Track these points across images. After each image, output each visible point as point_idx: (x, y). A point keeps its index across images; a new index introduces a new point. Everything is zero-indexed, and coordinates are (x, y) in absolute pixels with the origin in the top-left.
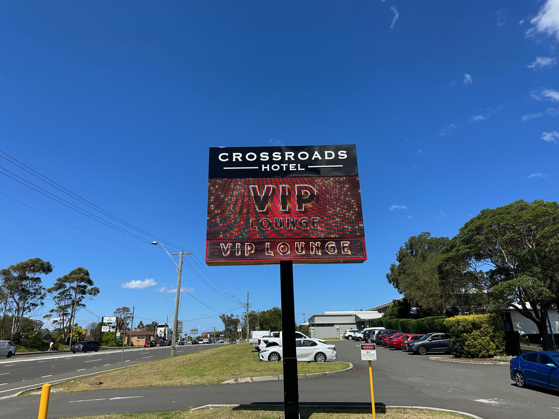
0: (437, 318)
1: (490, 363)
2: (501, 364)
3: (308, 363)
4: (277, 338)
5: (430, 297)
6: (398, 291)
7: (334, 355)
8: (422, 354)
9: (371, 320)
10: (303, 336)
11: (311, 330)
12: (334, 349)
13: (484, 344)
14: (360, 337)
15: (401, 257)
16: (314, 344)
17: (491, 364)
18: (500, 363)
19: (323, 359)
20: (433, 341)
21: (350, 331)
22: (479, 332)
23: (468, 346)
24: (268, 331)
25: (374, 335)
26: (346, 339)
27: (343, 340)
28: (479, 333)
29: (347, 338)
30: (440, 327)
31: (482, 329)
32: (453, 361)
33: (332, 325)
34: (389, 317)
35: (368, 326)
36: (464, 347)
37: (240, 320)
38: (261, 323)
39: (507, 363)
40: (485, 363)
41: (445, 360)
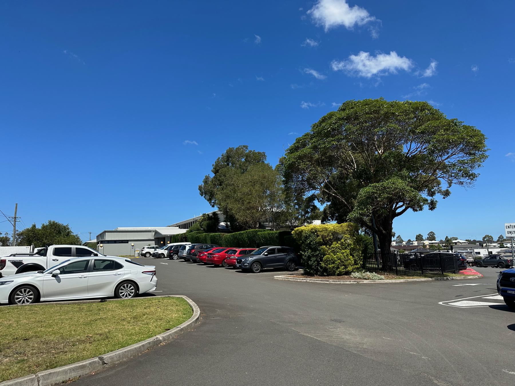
0: (259, 231)
1: (353, 282)
2: (364, 282)
3: (101, 302)
4: (42, 257)
5: (248, 209)
6: (211, 205)
7: (153, 283)
8: (255, 271)
9: (172, 236)
10: (93, 253)
11: (100, 248)
12: (154, 273)
13: (343, 259)
14: (163, 254)
15: (218, 168)
16: (116, 266)
17: (354, 283)
18: (363, 281)
19: (132, 293)
20: (269, 256)
21: (148, 248)
22: (339, 244)
23: (326, 261)
24: (30, 247)
25: (184, 250)
26: (142, 257)
27: (138, 257)
28: (340, 246)
29: (144, 255)
30: (263, 240)
31: (343, 240)
32: (308, 281)
33: (126, 242)
34: (197, 232)
35: (169, 242)
36: (321, 262)
37: (10, 239)
38: (29, 239)
39: (370, 282)
40: (347, 283)
41: (297, 279)
